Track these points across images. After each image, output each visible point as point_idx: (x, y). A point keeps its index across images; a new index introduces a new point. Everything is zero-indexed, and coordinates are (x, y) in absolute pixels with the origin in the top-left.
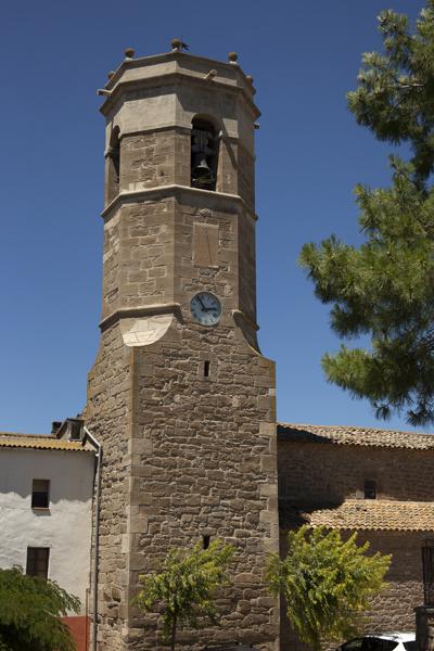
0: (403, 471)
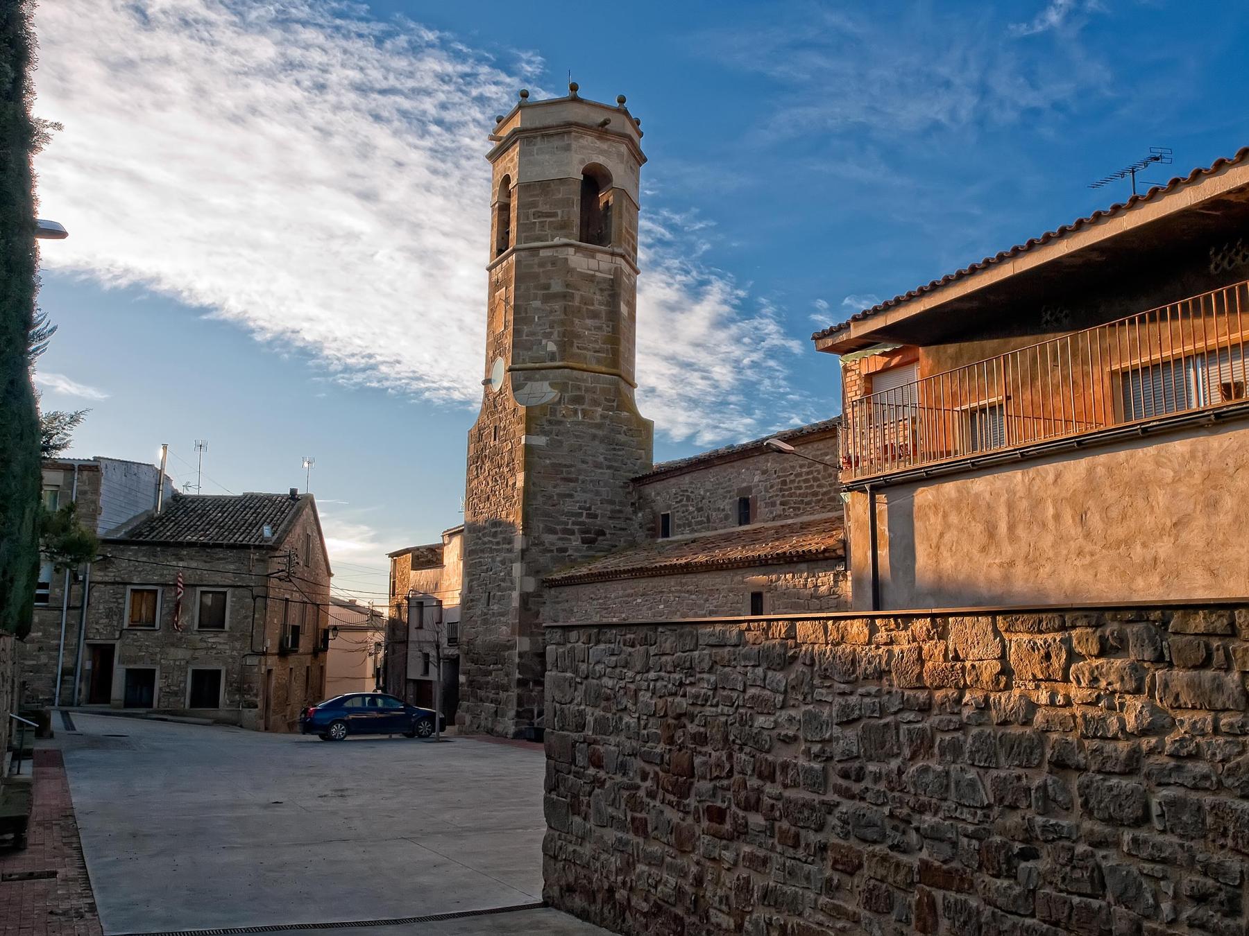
0: (779, 477)
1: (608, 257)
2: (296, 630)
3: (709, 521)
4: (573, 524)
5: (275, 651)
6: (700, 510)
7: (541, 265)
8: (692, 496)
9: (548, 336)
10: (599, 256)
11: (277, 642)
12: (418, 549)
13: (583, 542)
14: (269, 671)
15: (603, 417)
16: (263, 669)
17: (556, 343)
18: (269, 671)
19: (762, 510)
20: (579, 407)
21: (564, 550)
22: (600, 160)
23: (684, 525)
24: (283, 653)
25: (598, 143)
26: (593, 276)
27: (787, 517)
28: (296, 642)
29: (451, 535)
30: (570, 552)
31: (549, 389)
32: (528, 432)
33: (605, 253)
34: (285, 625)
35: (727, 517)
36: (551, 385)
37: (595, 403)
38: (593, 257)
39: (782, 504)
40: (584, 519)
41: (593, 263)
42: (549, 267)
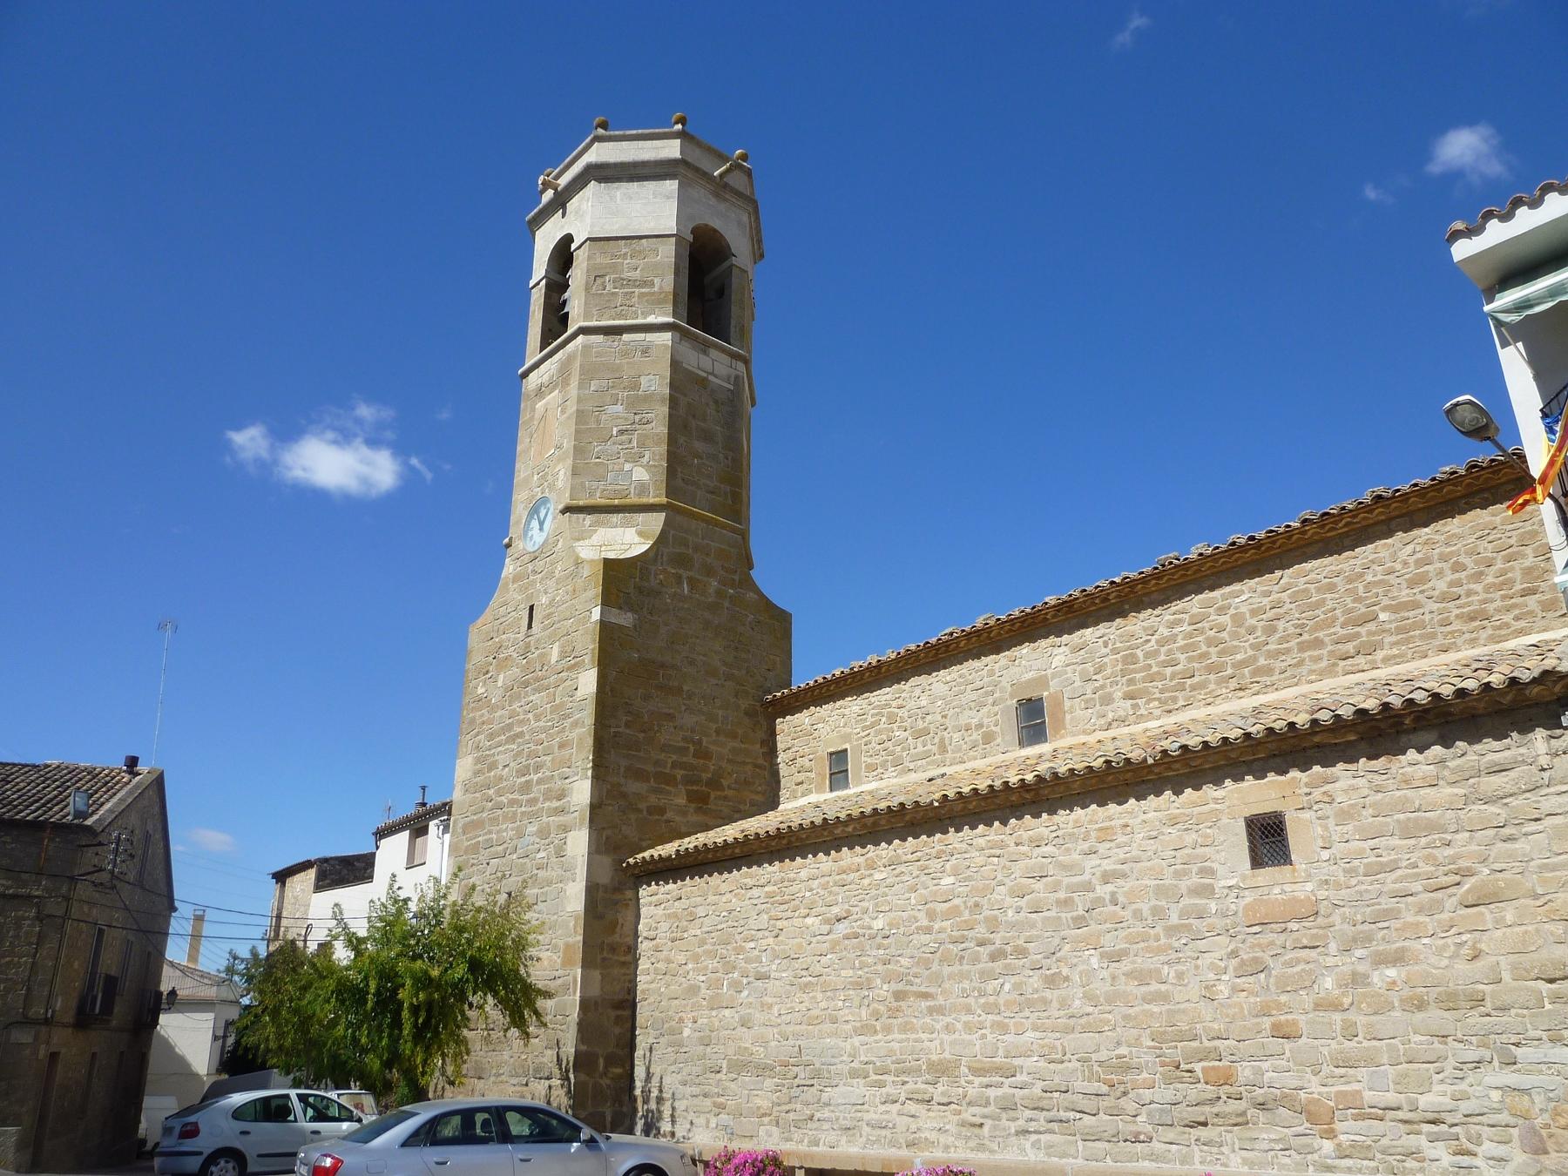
0: (1115, 651)
1: (726, 359)
2: (111, 982)
3: (943, 749)
4: (674, 765)
5: (69, 1018)
6: (920, 734)
7: (625, 354)
8: (902, 713)
9: (636, 459)
10: (714, 353)
11: (73, 1003)
12: (326, 860)
13: (690, 800)
14: (54, 1056)
15: (719, 593)
16: (42, 1053)
17: (647, 467)
18: (54, 1056)
19: (1075, 713)
20: (685, 574)
21: (661, 811)
22: (716, 224)
23: (884, 765)
24: (84, 1019)
25: (713, 201)
26: (705, 379)
27: (1141, 719)
28: (108, 1007)
29: (382, 833)
30: (669, 815)
31: (637, 539)
32: (606, 603)
33: (723, 350)
34: (93, 974)
35: (988, 738)
36: (640, 534)
37: (709, 571)
38: (705, 353)
39: (1129, 696)
40: (689, 759)
41: (705, 362)
42: (638, 357)
